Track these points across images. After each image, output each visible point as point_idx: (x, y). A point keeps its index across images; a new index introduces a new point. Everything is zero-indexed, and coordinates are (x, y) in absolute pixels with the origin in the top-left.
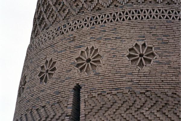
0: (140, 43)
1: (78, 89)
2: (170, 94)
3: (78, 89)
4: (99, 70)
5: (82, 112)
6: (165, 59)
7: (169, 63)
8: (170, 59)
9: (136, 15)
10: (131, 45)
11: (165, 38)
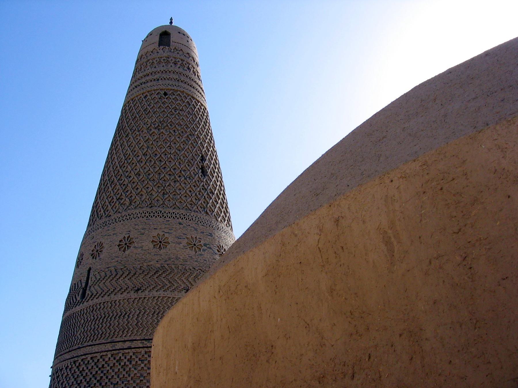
0: (127, 236)
1: (90, 269)
2: (139, 267)
3: (90, 269)
4: (102, 256)
5: (89, 284)
6: (140, 245)
7: (142, 247)
8: (143, 244)
9: (128, 217)
10: (121, 237)
11: (143, 231)
